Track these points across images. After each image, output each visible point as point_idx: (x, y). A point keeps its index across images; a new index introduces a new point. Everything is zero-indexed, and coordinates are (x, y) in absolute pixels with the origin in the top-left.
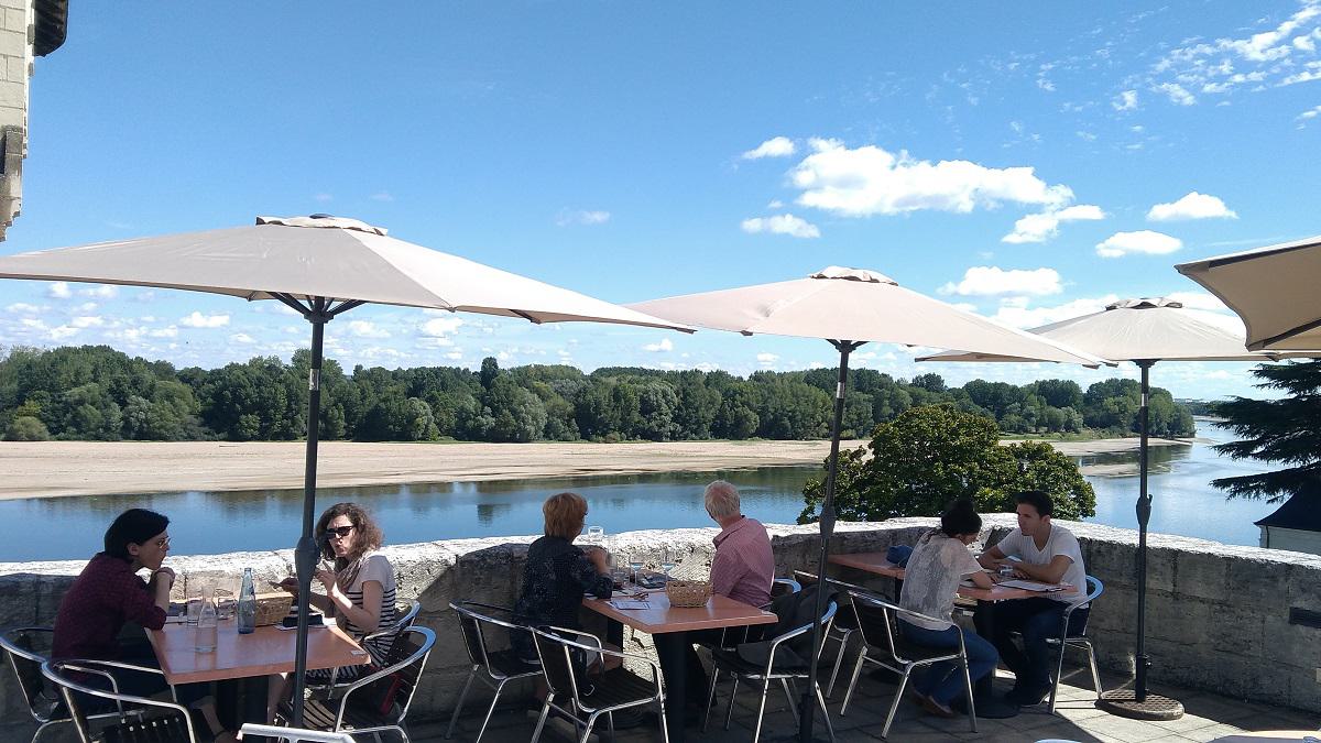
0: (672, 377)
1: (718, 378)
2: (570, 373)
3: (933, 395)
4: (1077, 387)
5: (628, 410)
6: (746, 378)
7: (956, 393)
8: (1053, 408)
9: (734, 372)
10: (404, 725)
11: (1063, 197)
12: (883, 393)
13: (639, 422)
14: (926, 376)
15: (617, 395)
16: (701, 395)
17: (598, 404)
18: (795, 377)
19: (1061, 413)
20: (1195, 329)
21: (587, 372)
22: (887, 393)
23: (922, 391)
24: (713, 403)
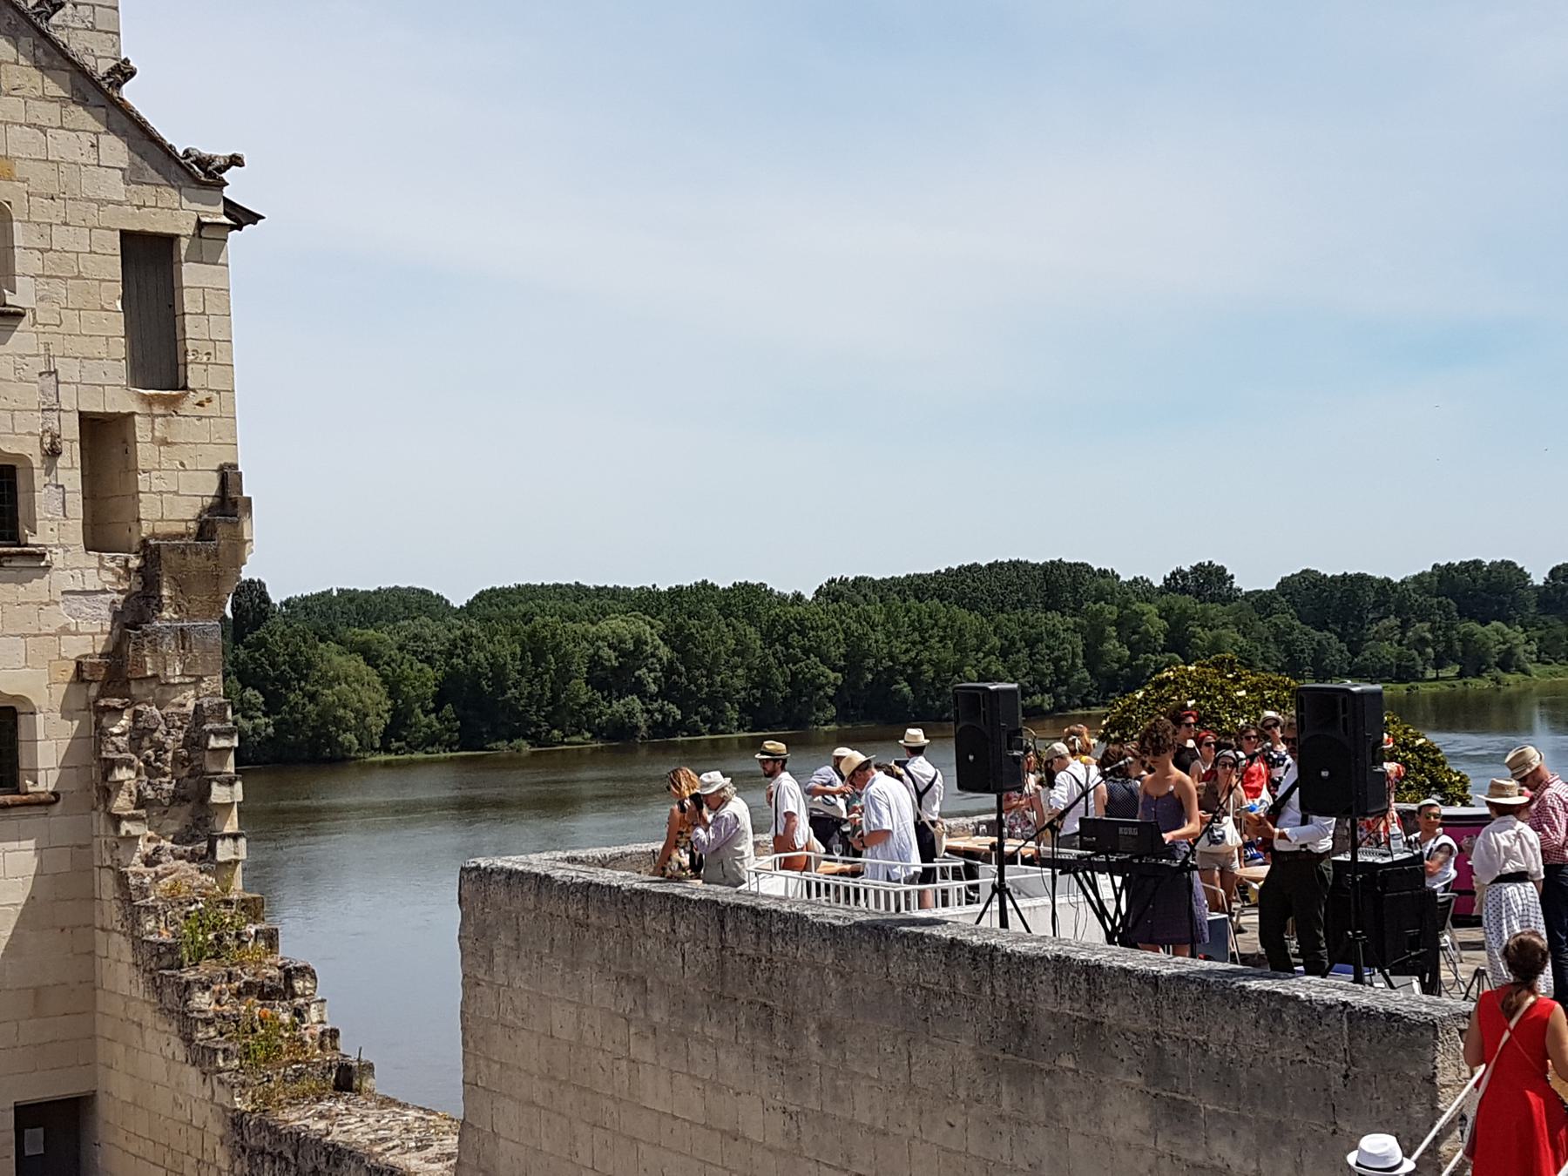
0: (646, 601)
1: (749, 598)
2: (421, 603)
3: (1214, 609)
4: (1522, 575)
5: (564, 675)
6: (809, 596)
7: (1261, 601)
8: (1474, 626)
9: (783, 585)
10: (1541, 885)
11: (162, 619)
12: (1101, 611)
13: (590, 704)
14: (1195, 569)
15: (536, 649)
16: (718, 636)
17: (498, 670)
18: (917, 587)
19: (1491, 633)
20: (564, 782)
21: (458, 600)
22: (1111, 612)
23: (1186, 601)
24: (741, 654)
